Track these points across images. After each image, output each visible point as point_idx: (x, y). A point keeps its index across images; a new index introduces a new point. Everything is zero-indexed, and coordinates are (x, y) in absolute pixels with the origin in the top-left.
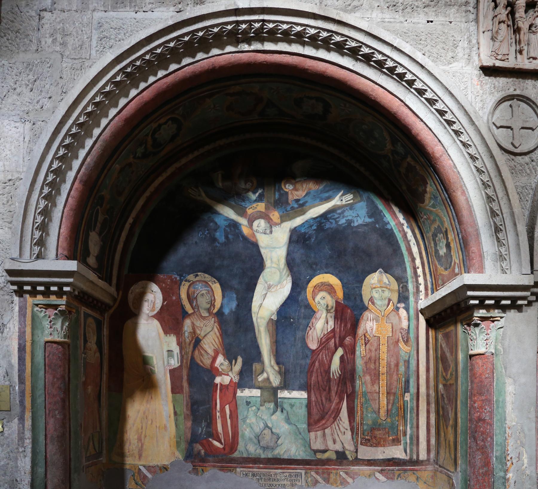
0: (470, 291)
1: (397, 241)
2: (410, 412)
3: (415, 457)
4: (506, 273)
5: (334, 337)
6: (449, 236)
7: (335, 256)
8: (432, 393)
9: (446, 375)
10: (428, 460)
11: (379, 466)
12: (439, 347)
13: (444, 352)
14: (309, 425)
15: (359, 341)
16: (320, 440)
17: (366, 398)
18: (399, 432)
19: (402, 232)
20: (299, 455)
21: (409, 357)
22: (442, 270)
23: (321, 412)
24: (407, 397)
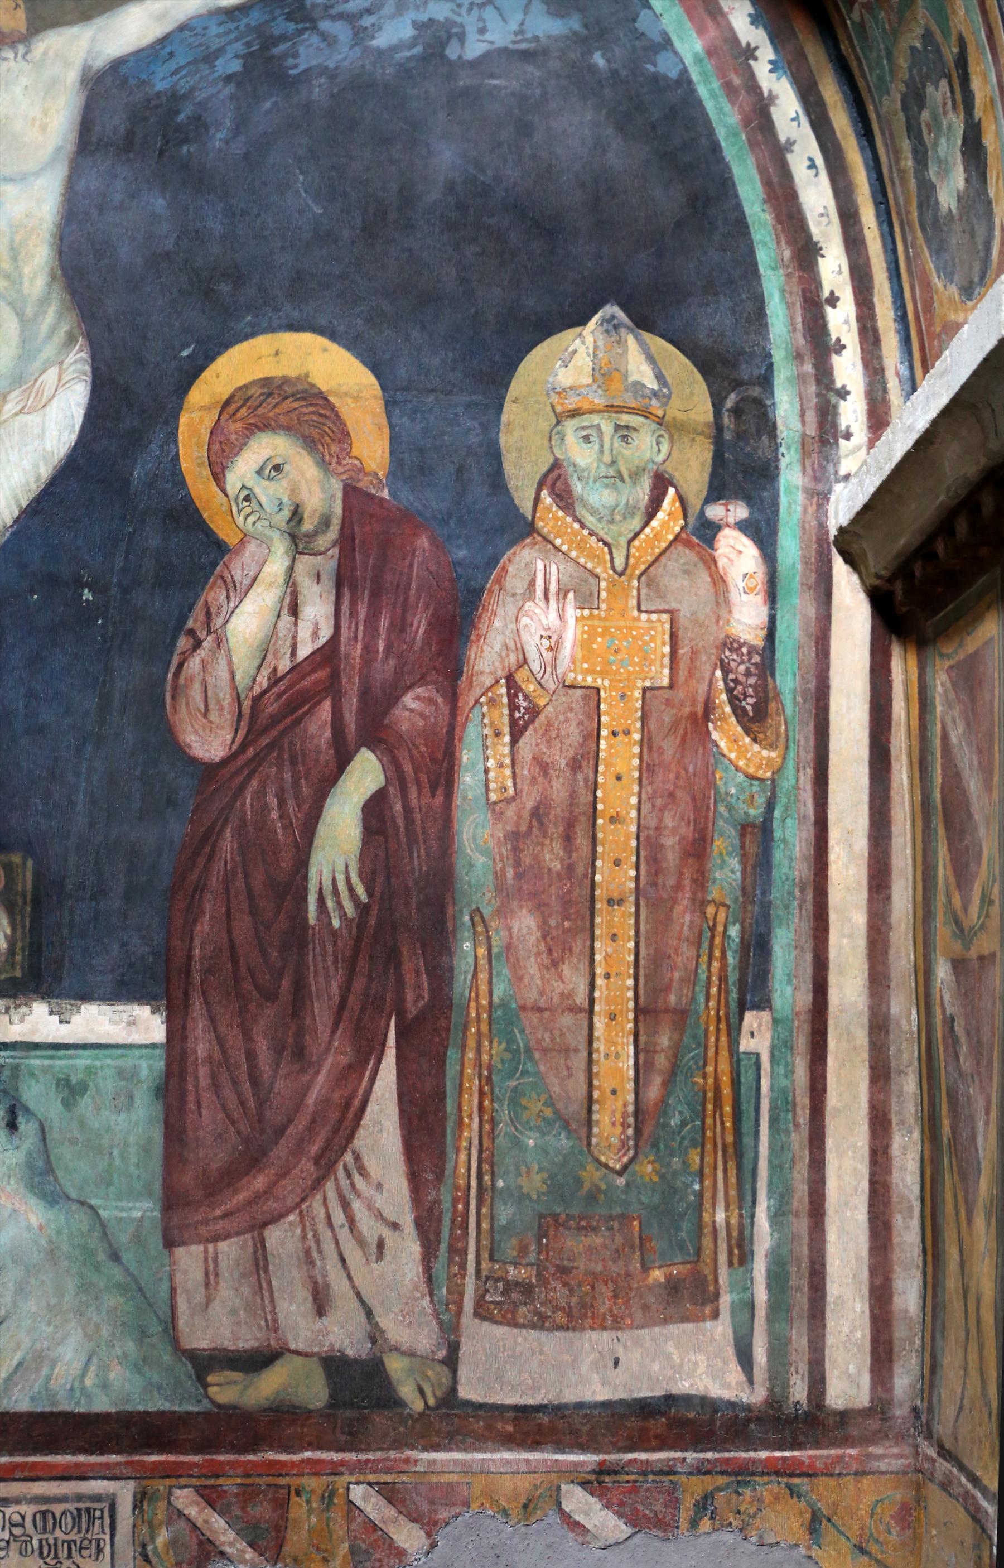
1: (715, 148)
2: (774, 1121)
3: (799, 1391)
5: (333, 688)
6: (976, 84)
7: (346, 234)
8: (902, 1008)
10: (880, 1406)
11: (583, 1448)
12: (937, 742)
13: (958, 775)
14: (172, 1200)
15: (475, 715)
16: (229, 1293)
17: (511, 1040)
18: (707, 1242)
19: (743, 95)
20: (104, 1386)
21: (770, 806)
23: (244, 1127)
24: (757, 1034)
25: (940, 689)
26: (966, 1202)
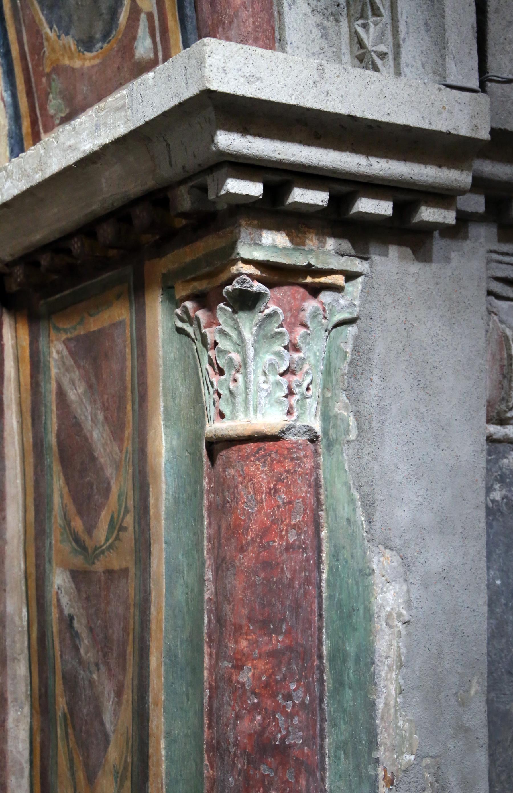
0: (229, 129)
4: (376, 69)
9: (90, 530)
12: (52, 398)
13: (77, 426)
22: (65, 48)
25: (55, 355)
26: (86, 765)
